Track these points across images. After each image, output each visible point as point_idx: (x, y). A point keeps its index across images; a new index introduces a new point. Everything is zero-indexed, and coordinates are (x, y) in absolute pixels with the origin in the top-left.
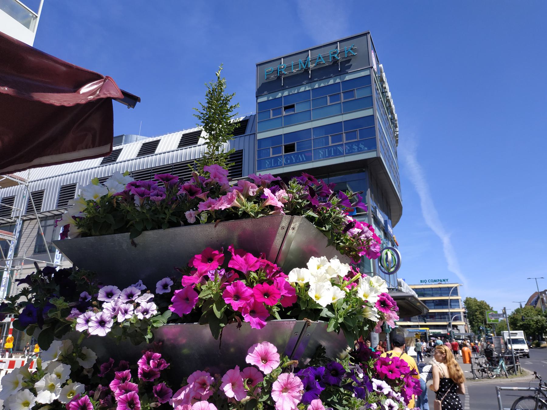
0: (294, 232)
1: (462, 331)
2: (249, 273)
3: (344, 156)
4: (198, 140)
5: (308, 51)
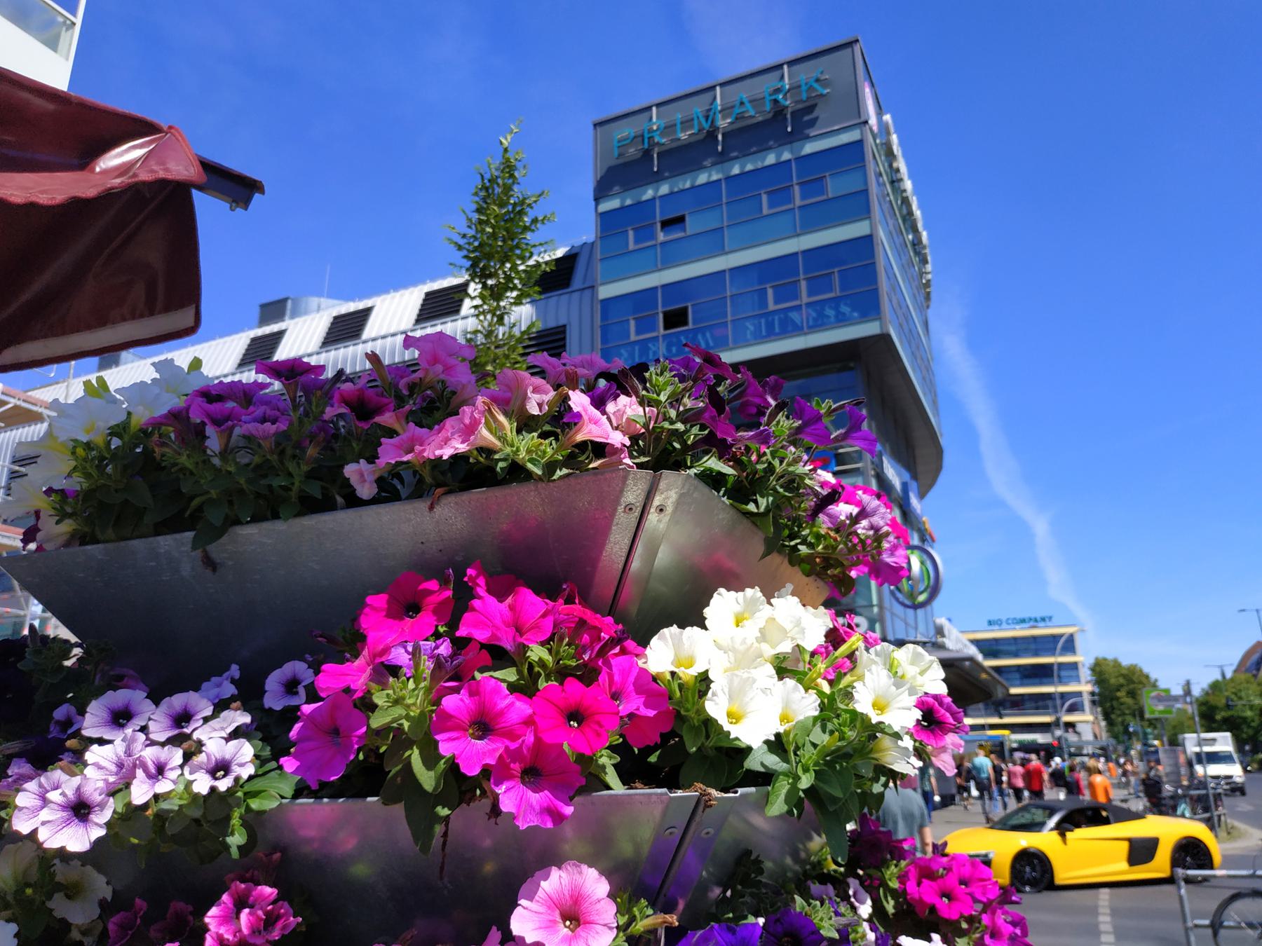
0: (663, 521)
1: (1088, 735)
2: (523, 649)
3: (806, 334)
4: (460, 306)
5: (713, 88)
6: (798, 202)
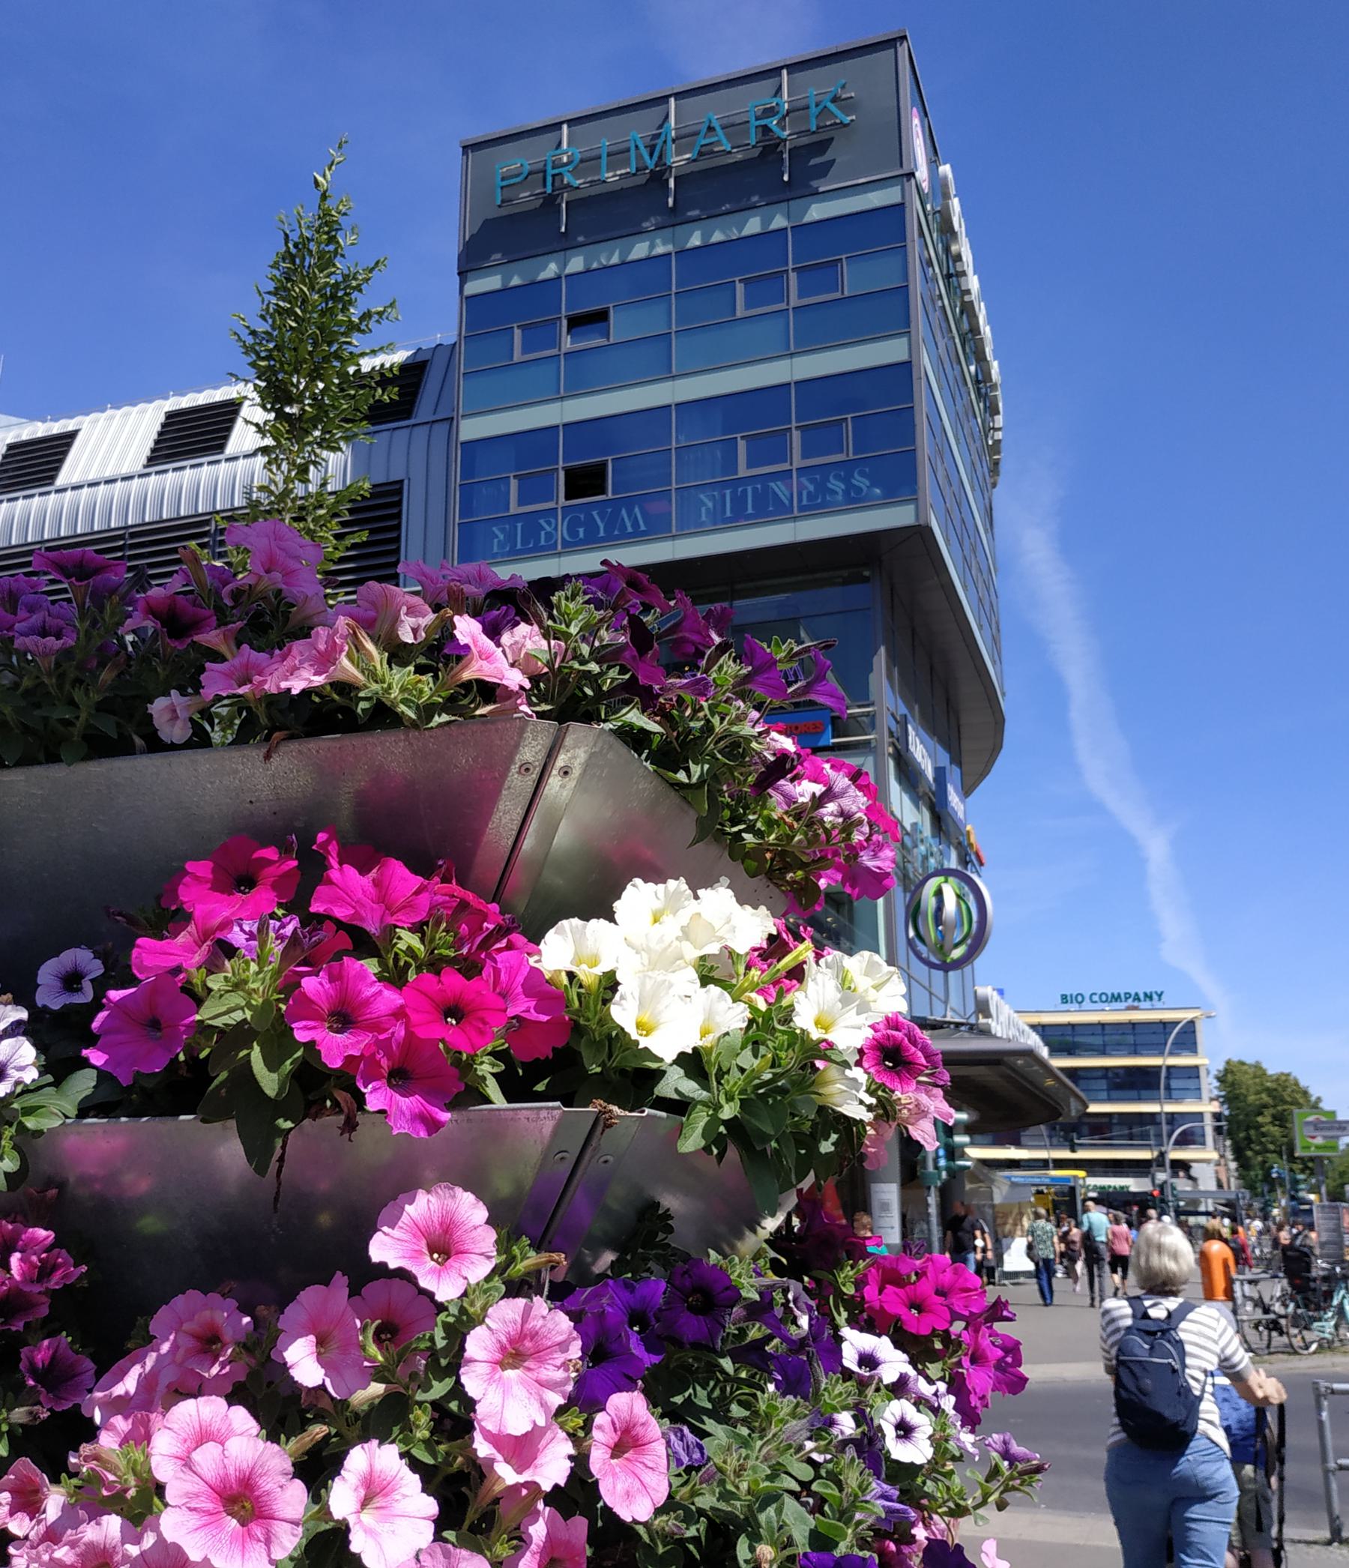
0: (568, 787)
1: (1207, 1184)
3: (795, 519)
5: (664, 99)
6: (794, 301)
